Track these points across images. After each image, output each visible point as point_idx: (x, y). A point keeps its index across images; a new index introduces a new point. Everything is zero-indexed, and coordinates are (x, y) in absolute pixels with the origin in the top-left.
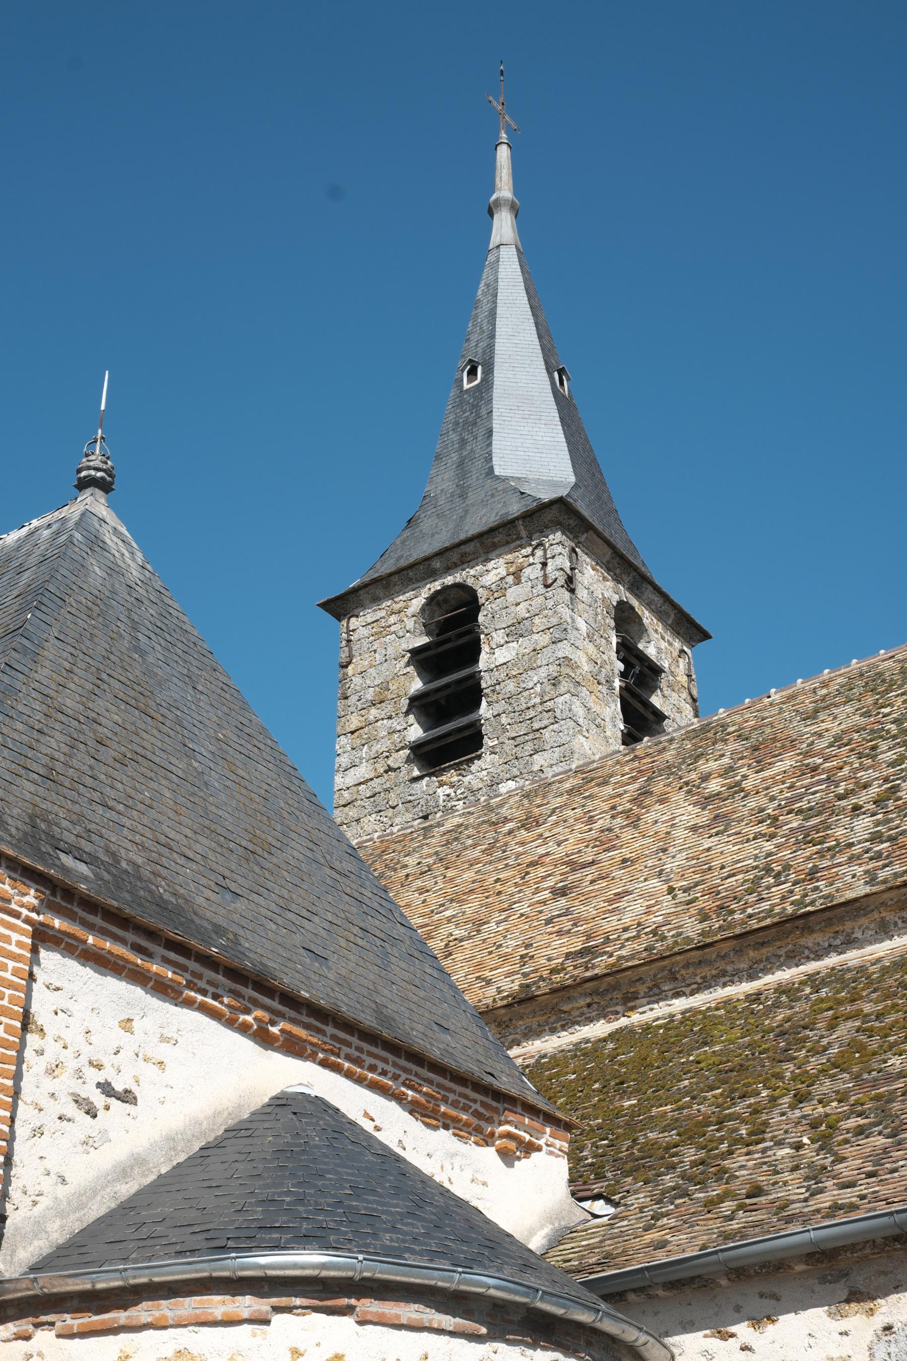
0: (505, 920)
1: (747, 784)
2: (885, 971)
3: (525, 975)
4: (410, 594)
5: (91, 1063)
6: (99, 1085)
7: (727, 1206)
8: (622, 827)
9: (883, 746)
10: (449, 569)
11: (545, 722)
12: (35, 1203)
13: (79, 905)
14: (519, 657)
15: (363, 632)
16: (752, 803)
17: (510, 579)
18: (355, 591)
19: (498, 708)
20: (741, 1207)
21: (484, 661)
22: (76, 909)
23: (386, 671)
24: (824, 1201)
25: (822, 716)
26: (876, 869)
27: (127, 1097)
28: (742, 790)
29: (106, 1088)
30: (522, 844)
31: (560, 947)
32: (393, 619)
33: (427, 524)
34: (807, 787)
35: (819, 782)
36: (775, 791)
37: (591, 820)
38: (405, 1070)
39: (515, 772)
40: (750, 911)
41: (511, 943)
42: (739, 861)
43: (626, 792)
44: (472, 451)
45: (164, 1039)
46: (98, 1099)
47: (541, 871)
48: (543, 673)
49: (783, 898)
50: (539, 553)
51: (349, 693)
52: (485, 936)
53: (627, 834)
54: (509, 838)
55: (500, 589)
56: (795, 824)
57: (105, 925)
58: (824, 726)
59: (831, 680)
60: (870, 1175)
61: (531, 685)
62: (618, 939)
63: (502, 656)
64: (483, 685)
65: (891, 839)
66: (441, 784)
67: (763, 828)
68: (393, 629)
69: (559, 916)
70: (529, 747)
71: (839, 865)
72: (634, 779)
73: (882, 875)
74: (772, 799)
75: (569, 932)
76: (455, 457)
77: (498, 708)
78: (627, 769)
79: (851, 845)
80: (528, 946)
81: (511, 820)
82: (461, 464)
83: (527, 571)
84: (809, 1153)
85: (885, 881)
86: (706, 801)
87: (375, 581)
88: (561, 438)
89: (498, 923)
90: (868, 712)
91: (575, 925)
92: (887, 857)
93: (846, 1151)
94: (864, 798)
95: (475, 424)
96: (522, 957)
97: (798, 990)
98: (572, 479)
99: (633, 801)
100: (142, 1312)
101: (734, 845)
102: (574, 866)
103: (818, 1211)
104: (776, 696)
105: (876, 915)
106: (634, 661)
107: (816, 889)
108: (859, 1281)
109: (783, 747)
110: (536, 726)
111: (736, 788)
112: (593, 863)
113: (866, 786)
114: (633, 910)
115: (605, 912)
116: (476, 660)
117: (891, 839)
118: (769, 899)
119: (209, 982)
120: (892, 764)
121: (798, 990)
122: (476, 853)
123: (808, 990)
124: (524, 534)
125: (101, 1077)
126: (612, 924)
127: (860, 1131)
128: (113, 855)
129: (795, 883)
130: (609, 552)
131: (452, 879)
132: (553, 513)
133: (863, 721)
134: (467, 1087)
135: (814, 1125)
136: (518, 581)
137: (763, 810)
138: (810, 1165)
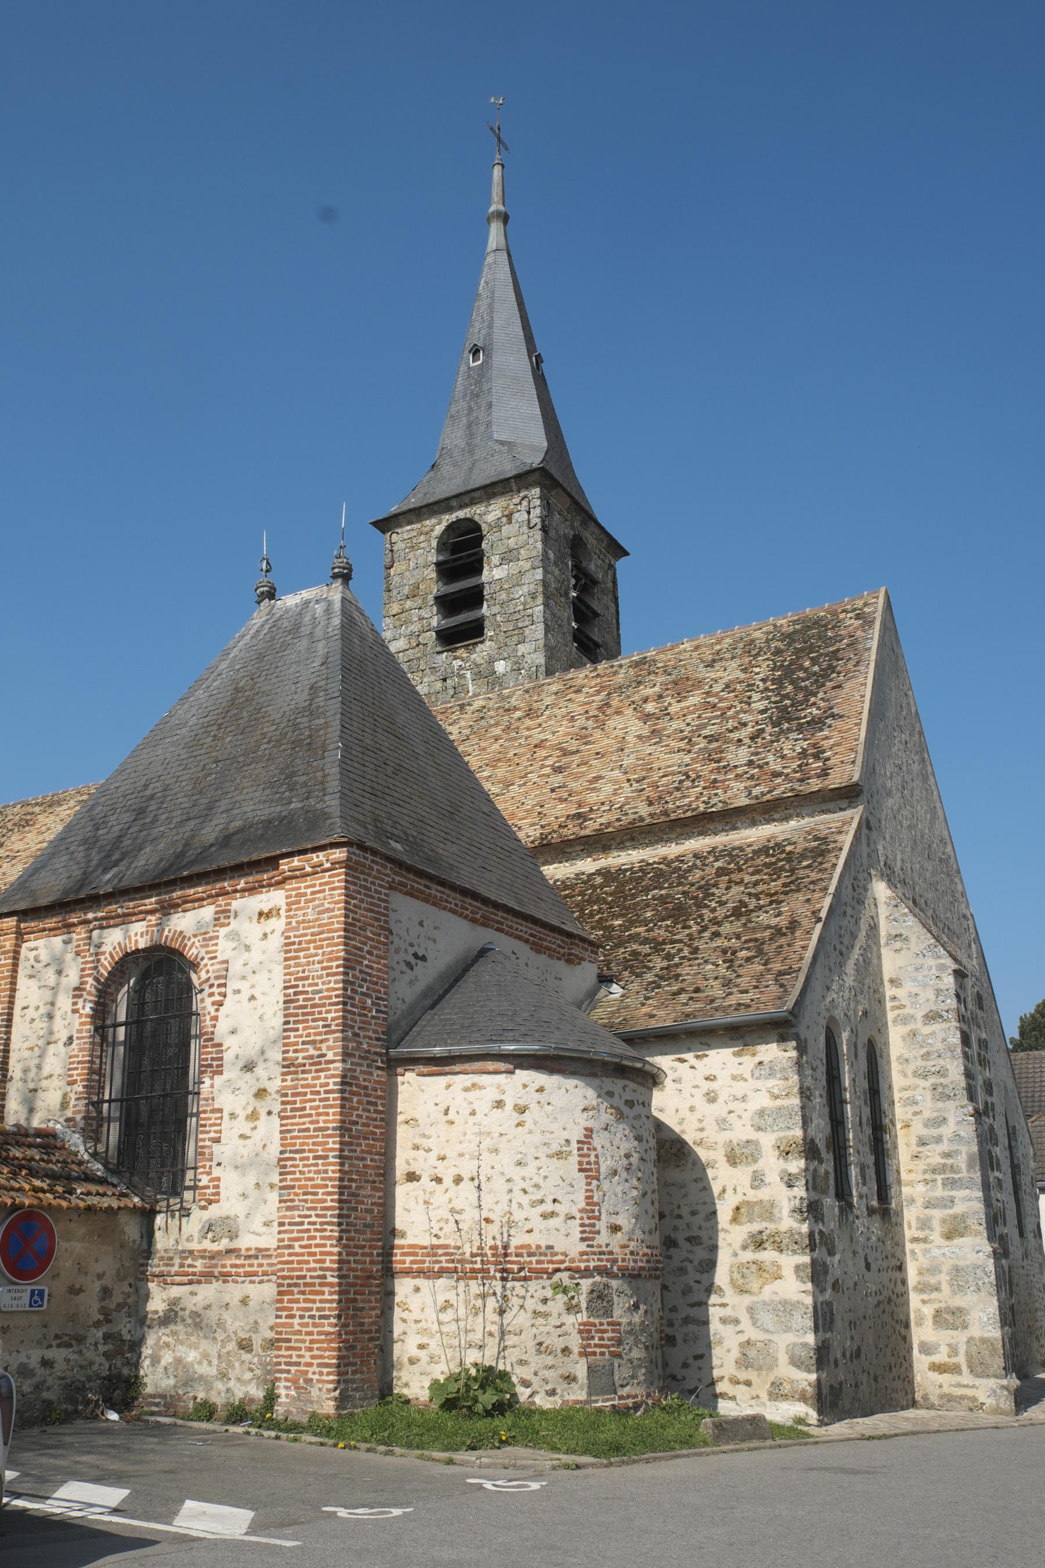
0: (525, 784)
1: (672, 710)
2: (757, 853)
3: (542, 827)
4: (434, 521)
7: (683, 998)
8: (593, 728)
9: (756, 697)
10: (461, 507)
11: (527, 623)
14: (509, 577)
15: (402, 545)
16: (675, 725)
17: (504, 520)
18: (396, 516)
19: (496, 609)
20: (691, 998)
21: (485, 576)
23: (418, 575)
24: (733, 1000)
25: (717, 666)
26: (751, 786)
27: (424, 958)
28: (668, 714)
29: (415, 955)
30: (528, 729)
31: (561, 810)
32: (422, 538)
33: (446, 469)
34: (710, 719)
35: (716, 717)
36: (689, 720)
37: (572, 719)
38: (531, 929)
39: (506, 655)
40: (678, 803)
41: (530, 803)
42: (669, 767)
43: (593, 701)
44: (477, 418)
45: (435, 928)
46: (413, 961)
47: (543, 753)
48: (525, 589)
49: (697, 798)
50: (525, 503)
51: (391, 587)
52: (512, 794)
53: (598, 734)
54: (519, 724)
55: (497, 526)
56: (702, 746)
58: (719, 674)
59: (722, 639)
60: (756, 987)
61: (517, 596)
62: (598, 809)
63: (498, 573)
64: (485, 593)
65: (760, 767)
66: (455, 658)
67: (682, 745)
68: (422, 545)
69: (559, 787)
70: (515, 639)
71: (729, 780)
72: (598, 692)
73: (756, 792)
74: (688, 725)
75: (566, 800)
76: (464, 420)
77: (496, 609)
78: (593, 683)
79: (736, 767)
80: (542, 806)
81: (519, 709)
82: (469, 426)
83: (516, 516)
84: (722, 971)
85: (756, 797)
86: (646, 717)
87: (410, 511)
88: (538, 411)
89: (520, 786)
90: (746, 669)
91: (570, 795)
92: (758, 779)
93: (741, 971)
94: (744, 733)
95: (478, 396)
96: (539, 813)
97: (706, 858)
98: (545, 444)
99: (600, 708)
100: (457, 1068)
101: (666, 754)
102: (565, 753)
103: (731, 1005)
104: (687, 646)
105: (750, 815)
106: (581, 576)
107: (716, 794)
109: (693, 685)
110: (520, 625)
111: (665, 712)
112: (578, 751)
113: (745, 725)
114: (607, 789)
115: (588, 789)
116: (479, 571)
117: (760, 767)
118: (689, 797)
120: (762, 712)
121: (706, 858)
122: (497, 731)
123: (711, 859)
124: (514, 488)
126: (592, 798)
127: (748, 960)
128: (405, 833)
129: (704, 788)
130: (569, 501)
131: (484, 749)
132: (536, 476)
133: (742, 676)
135: (724, 952)
136: (510, 521)
137: (682, 731)
138: (724, 977)
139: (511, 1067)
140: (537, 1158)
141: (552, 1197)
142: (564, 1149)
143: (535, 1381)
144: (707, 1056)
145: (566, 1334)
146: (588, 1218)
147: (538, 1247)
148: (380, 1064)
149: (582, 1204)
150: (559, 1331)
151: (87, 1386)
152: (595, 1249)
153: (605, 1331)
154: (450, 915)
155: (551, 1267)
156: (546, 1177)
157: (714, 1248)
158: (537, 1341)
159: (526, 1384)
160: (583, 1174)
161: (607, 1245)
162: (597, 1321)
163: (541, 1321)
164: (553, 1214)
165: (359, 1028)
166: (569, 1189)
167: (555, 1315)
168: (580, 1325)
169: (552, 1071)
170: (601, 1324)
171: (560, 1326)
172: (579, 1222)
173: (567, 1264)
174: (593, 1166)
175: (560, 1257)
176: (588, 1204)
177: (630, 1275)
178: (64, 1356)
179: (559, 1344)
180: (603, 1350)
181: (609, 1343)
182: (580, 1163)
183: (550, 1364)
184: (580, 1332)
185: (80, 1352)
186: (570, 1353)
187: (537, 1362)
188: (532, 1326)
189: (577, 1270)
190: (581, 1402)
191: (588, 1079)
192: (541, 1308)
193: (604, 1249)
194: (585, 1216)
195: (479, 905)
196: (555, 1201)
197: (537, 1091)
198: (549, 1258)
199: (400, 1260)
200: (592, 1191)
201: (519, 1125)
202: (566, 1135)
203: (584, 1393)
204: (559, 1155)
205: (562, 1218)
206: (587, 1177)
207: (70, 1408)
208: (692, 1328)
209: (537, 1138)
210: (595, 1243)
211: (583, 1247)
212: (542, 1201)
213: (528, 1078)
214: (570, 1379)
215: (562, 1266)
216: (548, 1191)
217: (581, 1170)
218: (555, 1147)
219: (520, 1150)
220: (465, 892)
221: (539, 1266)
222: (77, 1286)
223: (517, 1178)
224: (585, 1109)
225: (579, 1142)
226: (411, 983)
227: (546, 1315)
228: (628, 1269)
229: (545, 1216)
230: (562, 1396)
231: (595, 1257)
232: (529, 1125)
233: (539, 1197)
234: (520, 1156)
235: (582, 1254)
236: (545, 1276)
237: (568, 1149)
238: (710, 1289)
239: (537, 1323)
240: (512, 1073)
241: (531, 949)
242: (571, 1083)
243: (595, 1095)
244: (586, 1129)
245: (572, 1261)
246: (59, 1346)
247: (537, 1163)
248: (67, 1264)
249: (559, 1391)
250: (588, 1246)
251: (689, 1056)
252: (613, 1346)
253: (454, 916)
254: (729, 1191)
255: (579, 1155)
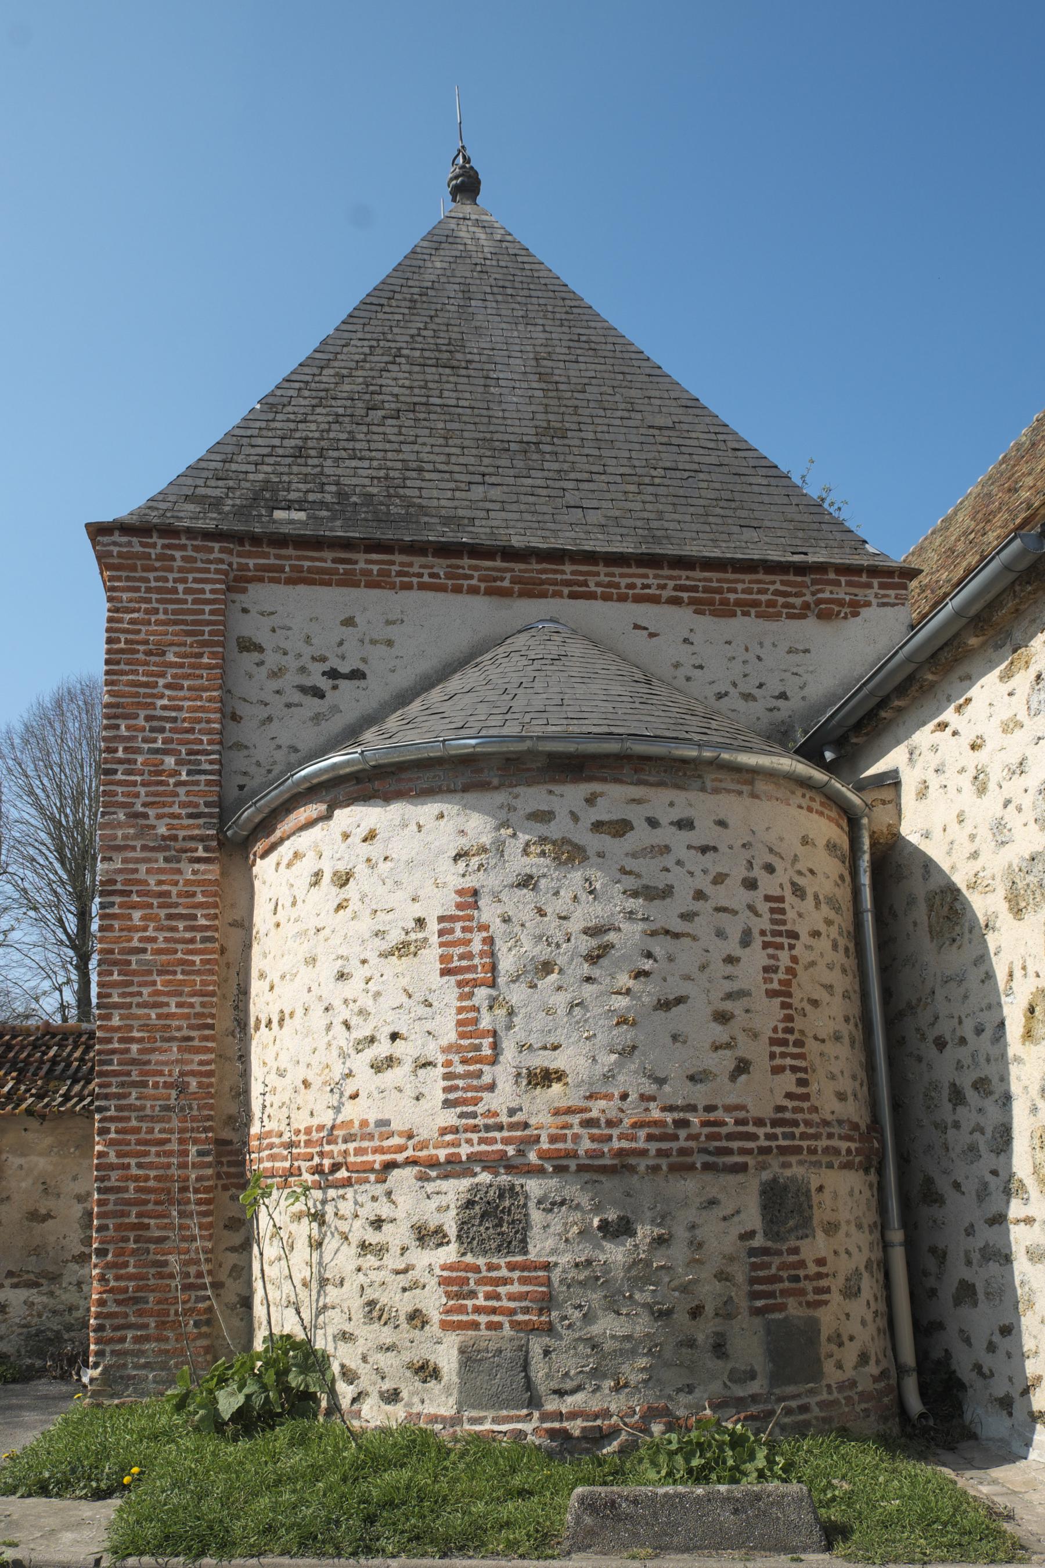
5: (313, 658)
6: (324, 674)
12: (269, 771)
13: (268, 546)
22: (267, 550)
29: (333, 674)
38: (671, 578)
45: (389, 623)
46: (324, 684)
57: (300, 553)
108: (1018, 635)
119: (421, 567)
125: (326, 666)
134: (757, 572)
139: (322, 807)
140: (364, 962)
141: (389, 1030)
142: (413, 936)
143: (364, 1371)
144: (968, 701)
145: (415, 1285)
146: (464, 1062)
147: (364, 1123)
148: (201, 853)
149: (450, 1036)
150: (403, 1280)
151: (66, 1337)
152: (479, 1121)
153: (505, 1281)
154: (429, 595)
155: (379, 1159)
156: (377, 994)
157: (1007, 1099)
158: (366, 1298)
159: (350, 1377)
160: (453, 979)
161: (512, 1112)
162: (481, 1261)
163: (371, 1260)
164: (390, 1062)
165: (144, 805)
166: (422, 1010)
167: (395, 1250)
168: (444, 1268)
169: (387, 798)
170: (491, 1267)
171: (405, 1271)
172: (440, 1070)
173: (409, 1153)
174: (477, 961)
175: (396, 1141)
176: (462, 1035)
177: (581, 1169)
178: (22, 1299)
179: (404, 1304)
180: (496, 1318)
181: (512, 1305)
182: (443, 959)
183: (389, 1341)
184: (444, 1282)
185: (51, 1294)
186: (424, 1323)
187: (369, 1335)
188: (359, 1270)
189: (433, 1163)
190: (443, 1420)
191: (470, 797)
192: (373, 1237)
193: (504, 1119)
194: (456, 1058)
195: (498, 564)
196: (394, 1036)
197: (365, 840)
198: (376, 1143)
199: (259, 1161)
200: (476, 1009)
201: (340, 907)
202: (417, 910)
203: (452, 1401)
204: (402, 949)
205: (407, 1067)
206: (460, 984)
207: (38, 1363)
208: (993, 1267)
209: (365, 925)
210: (480, 1109)
211: (450, 1118)
212: (372, 1040)
213: (349, 821)
214: (427, 1372)
215: (400, 1158)
216: (384, 1019)
217: (444, 972)
218: (395, 936)
219: (340, 952)
220: (446, 550)
221: (359, 1159)
222: (43, 1211)
223: (337, 1003)
224: (457, 857)
225: (441, 919)
226: (317, 718)
227: (380, 1250)
228: (575, 1155)
229: (380, 1066)
230: (409, 1405)
231: (475, 1137)
232: (354, 905)
233: (368, 1033)
234: (340, 962)
235: (444, 1131)
236: (372, 1177)
237: (420, 935)
238: (1008, 1188)
239: (365, 1266)
240: (328, 817)
241: (696, 612)
242: (426, 811)
243: (491, 822)
244: (460, 892)
245: (423, 1145)
246: (15, 1286)
247: (365, 971)
248: (23, 1185)
249: (404, 1394)
250: (462, 1116)
251: (949, 715)
252: (526, 1311)
253: (441, 595)
254: (1018, 973)
255: (442, 945)
